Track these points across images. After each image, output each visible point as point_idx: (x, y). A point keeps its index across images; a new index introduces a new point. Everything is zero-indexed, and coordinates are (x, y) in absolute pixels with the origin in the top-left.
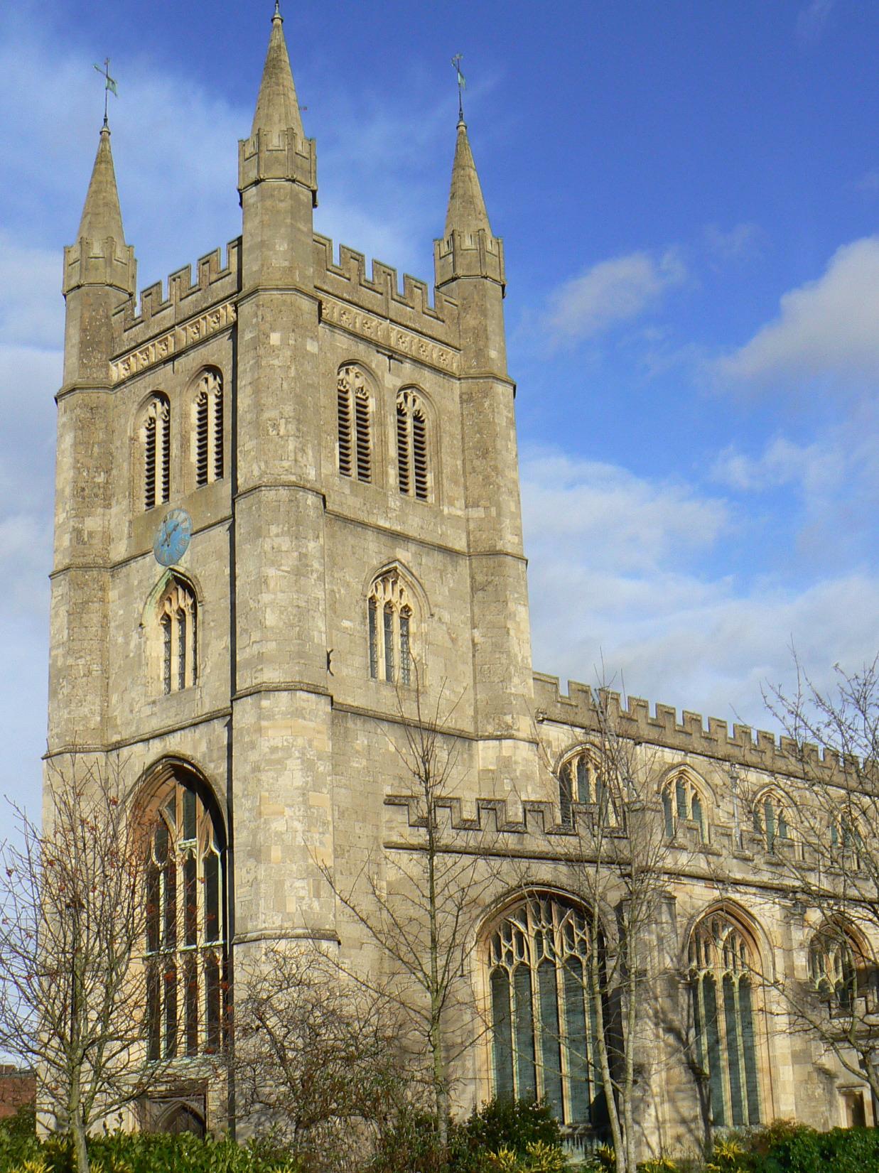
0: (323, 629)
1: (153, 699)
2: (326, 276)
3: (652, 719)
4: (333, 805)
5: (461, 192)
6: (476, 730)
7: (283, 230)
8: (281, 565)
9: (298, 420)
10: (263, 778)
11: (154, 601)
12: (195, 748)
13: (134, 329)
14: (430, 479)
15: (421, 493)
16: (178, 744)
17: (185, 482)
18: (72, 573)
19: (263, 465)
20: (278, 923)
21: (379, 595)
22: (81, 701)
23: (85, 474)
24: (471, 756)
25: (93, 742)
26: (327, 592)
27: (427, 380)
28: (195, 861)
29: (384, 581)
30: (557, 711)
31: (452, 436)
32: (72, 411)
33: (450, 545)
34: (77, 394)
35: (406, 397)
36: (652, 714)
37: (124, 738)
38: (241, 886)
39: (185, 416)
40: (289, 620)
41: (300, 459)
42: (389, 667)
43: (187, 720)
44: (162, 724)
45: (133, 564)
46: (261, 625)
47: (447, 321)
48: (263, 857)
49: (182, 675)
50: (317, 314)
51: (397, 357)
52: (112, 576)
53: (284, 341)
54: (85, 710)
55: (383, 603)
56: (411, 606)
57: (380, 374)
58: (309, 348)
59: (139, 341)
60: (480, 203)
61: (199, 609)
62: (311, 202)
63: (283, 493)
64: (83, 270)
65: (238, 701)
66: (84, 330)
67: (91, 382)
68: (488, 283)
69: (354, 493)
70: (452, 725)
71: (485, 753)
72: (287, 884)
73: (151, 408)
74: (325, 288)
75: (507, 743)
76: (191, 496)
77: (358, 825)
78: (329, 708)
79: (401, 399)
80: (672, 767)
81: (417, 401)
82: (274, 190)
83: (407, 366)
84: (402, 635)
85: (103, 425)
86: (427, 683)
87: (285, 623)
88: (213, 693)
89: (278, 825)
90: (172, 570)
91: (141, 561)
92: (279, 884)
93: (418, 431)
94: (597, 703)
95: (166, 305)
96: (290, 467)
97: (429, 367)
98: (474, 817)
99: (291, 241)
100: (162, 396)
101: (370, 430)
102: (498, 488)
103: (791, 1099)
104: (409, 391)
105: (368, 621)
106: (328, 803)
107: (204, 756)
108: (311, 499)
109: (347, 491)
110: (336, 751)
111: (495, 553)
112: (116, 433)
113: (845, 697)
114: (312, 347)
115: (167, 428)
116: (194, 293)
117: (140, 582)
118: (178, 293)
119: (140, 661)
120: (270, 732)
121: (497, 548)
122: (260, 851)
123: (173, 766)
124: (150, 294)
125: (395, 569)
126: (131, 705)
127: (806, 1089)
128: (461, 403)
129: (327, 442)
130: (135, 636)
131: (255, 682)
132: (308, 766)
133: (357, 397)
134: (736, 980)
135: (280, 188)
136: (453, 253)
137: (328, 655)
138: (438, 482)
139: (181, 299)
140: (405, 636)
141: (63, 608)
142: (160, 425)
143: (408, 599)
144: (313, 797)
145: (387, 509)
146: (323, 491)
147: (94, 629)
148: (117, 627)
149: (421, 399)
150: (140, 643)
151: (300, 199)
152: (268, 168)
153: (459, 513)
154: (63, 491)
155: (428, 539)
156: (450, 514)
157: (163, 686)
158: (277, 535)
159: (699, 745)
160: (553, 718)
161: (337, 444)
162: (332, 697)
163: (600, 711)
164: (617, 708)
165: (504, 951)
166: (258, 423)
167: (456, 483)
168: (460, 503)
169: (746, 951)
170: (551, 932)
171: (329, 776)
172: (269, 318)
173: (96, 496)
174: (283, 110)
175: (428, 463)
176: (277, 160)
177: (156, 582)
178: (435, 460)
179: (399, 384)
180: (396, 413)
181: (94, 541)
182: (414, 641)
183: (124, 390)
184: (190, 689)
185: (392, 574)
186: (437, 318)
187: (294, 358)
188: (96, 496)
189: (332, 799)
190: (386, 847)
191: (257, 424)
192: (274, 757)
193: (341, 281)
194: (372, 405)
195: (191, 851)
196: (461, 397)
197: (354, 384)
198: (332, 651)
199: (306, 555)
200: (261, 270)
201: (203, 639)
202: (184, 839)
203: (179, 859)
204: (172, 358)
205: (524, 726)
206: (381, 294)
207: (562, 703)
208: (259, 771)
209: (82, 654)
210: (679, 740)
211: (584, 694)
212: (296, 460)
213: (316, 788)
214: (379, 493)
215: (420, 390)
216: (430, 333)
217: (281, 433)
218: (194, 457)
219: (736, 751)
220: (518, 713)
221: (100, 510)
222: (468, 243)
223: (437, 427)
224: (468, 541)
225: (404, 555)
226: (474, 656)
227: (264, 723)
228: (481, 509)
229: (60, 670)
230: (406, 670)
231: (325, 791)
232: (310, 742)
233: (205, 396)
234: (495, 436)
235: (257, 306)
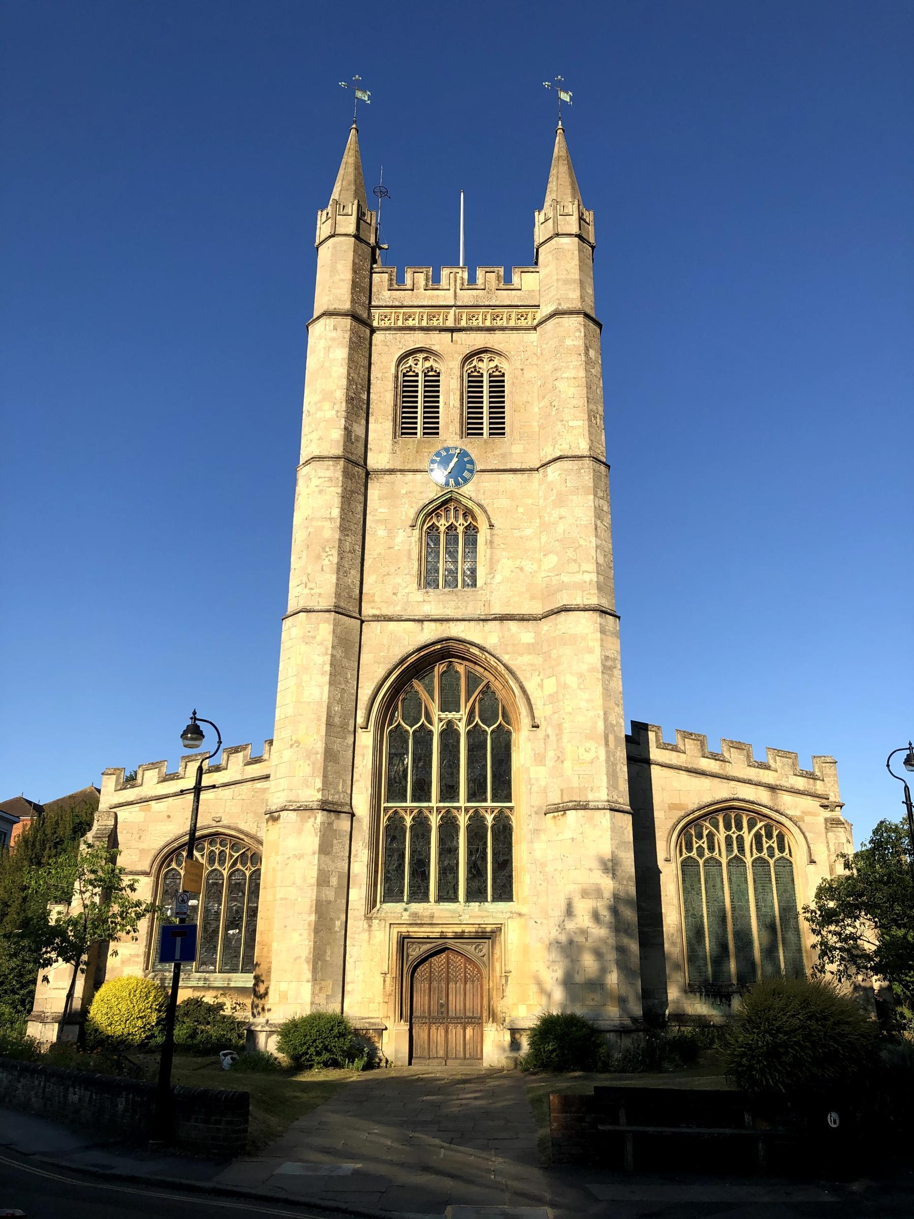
23: (354, 387)
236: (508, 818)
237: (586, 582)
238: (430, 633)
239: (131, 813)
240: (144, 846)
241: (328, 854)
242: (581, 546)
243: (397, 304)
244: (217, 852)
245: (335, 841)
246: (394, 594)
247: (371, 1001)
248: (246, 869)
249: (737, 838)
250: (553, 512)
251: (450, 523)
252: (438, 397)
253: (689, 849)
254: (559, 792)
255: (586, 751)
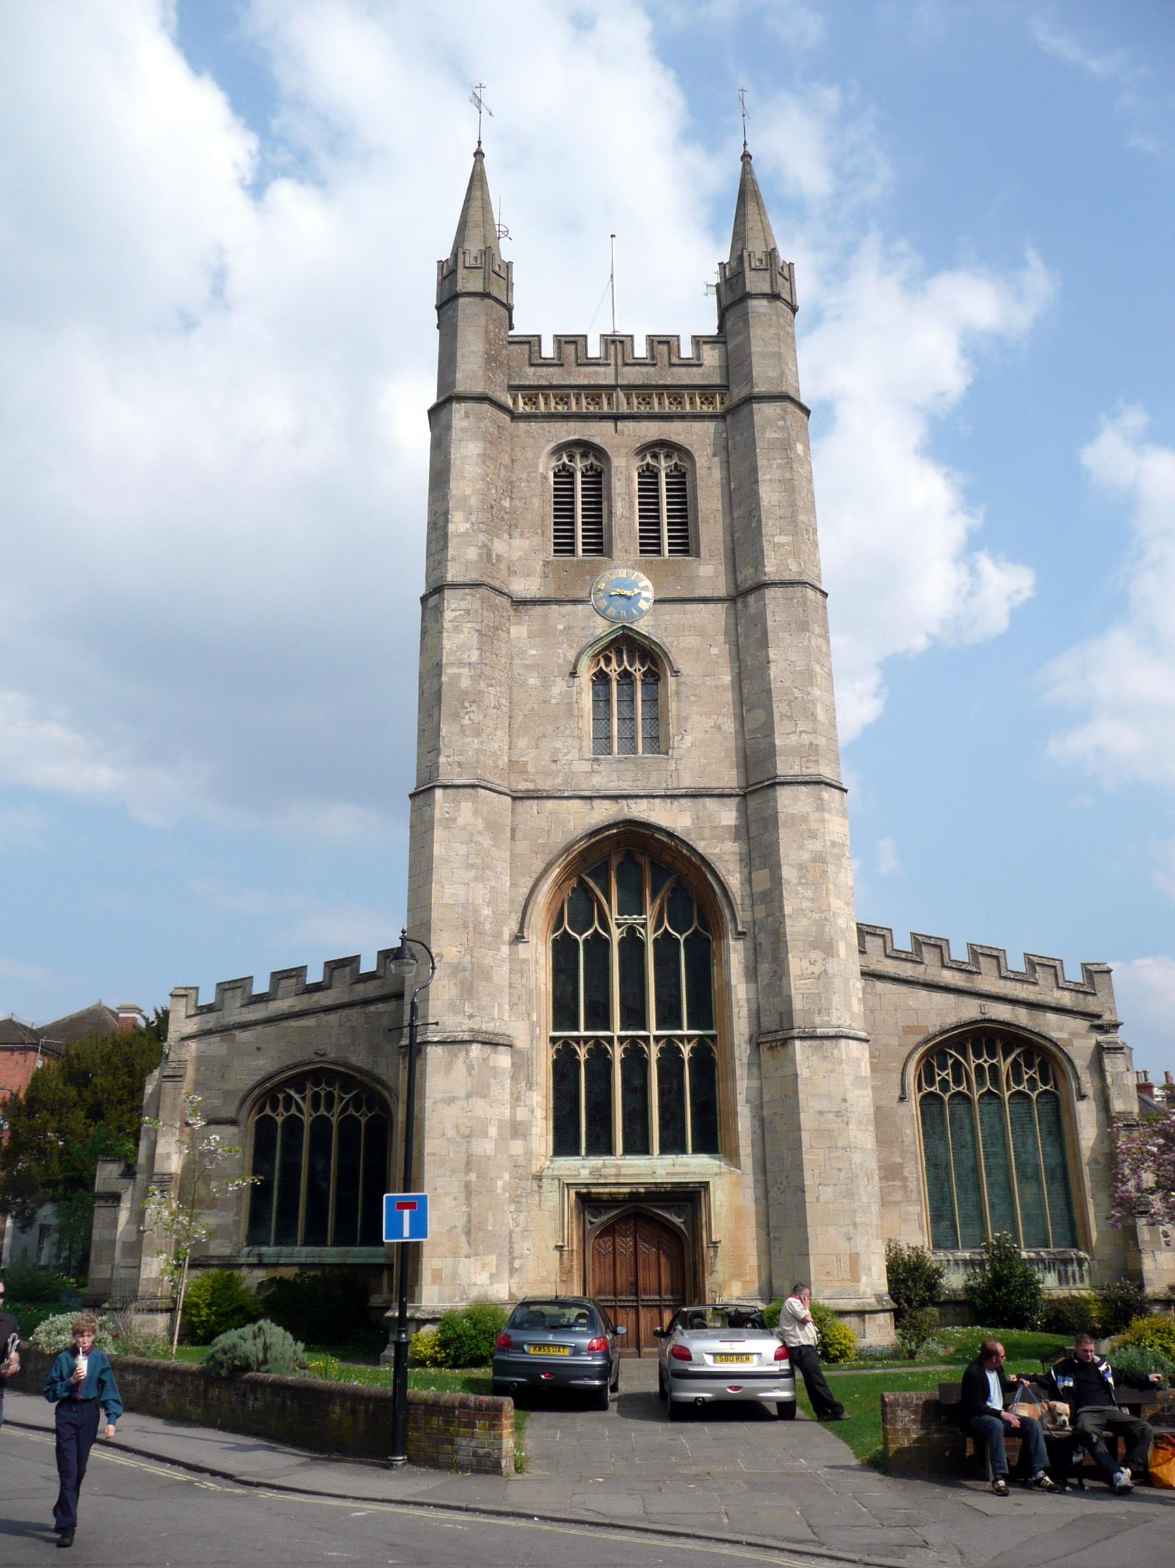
23: (494, 491)
236: (710, 1050)
237: (804, 746)
238: (603, 813)
239: (210, 1044)
240: (229, 1086)
241: (485, 1097)
242: (796, 698)
243: (544, 383)
244: (323, 1093)
245: (492, 1081)
246: (555, 761)
247: (544, 1281)
248: (361, 1115)
249: (989, 1067)
250: (758, 654)
251: (622, 668)
252: (641, 531)
253: (931, 1082)
254: (777, 1017)
255: (811, 964)
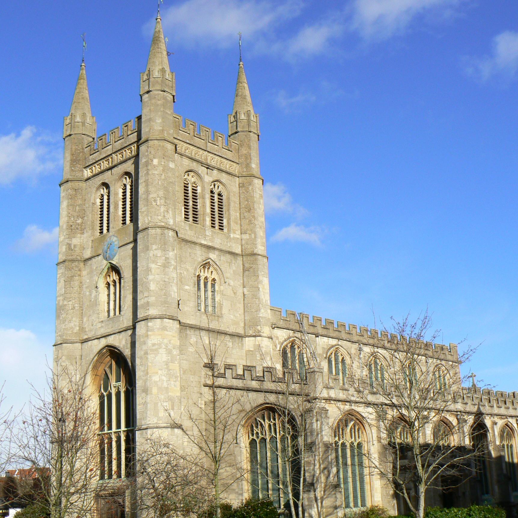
0: (176, 291)
1: (102, 320)
2: (179, 132)
3: (324, 325)
4: (180, 368)
5: (240, 94)
6: (245, 333)
7: (160, 113)
8: (157, 263)
9: (165, 198)
10: (149, 357)
11: (102, 276)
12: (120, 343)
13: (94, 155)
14: (225, 222)
15: (221, 228)
16: (112, 341)
17: (116, 223)
18: (66, 263)
19: (150, 219)
20: (155, 421)
21: (202, 274)
22: (70, 320)
23: (72, 219)
24: (242, 344)
25: (74, 339)
26: (178, 274)
27: (224, 178)
28: (120, 392)
29: (204, 267)
30: (281, 323)
31: (235, 202)
32: (67, 191)
33: (233, 251)
34: (69, 184)
35: (214, 185)
36: (323, 323)
37: (89, 337)
38: (139, 405)
39: (116, 194)
40: (161, 287)
41: (166, 215)
42: (206, 306)
43: (117, 330)
44: (106, 331)
45: (93, 260)
46: (148, 289)
47: (233, 151)
48: (149, 392)
49: (115, 310)
50: (174, 150)
51: (210, 168)
52: (84, 265)
53: (159, 163)
54: (72, 325)
55: (204, 277)
56: (216, 278)
57: (203, 175)
58: (171, 166)
59: (97, 160)
60: (249, 99)
61: (122, 281)
62: (172, 100)
63: (159, 231)
64: (72, 128)
65: (138, 323)
66: (73, 155)
67: (75, 177)
68: (251, 134)
69: (191, 229)
70: (234, 331)
71: (249, 343)
72: (160, 404)
73: (102, 190)
74: (179, 138)
75: (259, 338)
76: (119, 230)
77: (191, 376)
78: (178, 326)
79: (213, 186)
80: (333, 346)
81: (220, 187)
82: (156, 95)
83: (215, 171)
84: (212, 292)
85: (81, 197)
86: (223, 313)
87: (159, 289)
88: (126, 319)
89: (155, 378)
90: (110, 263)
91: (97, 258)
92: (156, 404)
93: (220, 203)
94: (299, 319)
95: (108, 144)
96: (162, 219)
97: (225, 172)
98: (241, 373)
99: (163, 118)
100: (106, 185)
101: (198, 201)
102: (255, 226)
103: (380, 495)
104: (216, 183)
105: (196, 286)
106: (178, 368)
107: (124, 346)
108: (171, 233)
109: (188, 228)
110: (182, 344)
111: (254, 254)
112: (86, 201)
113: (396, 330)
114: (172, 165)
115: (108, 199)
116: (121, 139)
117: (97, 267)
118: (114, 139)
119: (96, 303)
120: (152, 337)
121: (255, 252)
122: (147, 389)
123: (110, 350)
124: (102, 139)
125: (209, 262)
126: (92, 322)
127: (386, 491)
128: (239, 188)
129: (178, 207)
130: (94, 292)
131: (146, 314)
132: (169, 352)
133: (193, 186)
134: (356, 444)
135: (158, 94)
136: (236, 121)
137: (179, 301)
138: (229, 223)
139: (115, 142)
140: (213, 292)
141: (62, 279)
142: (106, 198)
143: (215, 276)
144: (171, 366)
145: (205, 236)
146: (177, 229)
147: (76, 288)
148: (87, 287)
149: (222, 186)
150: (96, 295)
151: (167, 99)
152: (153, 86)
153: (238, 236)
154: (63, 226)
155: (224, 248)
156: (234, 237)
157: (106, 314)
158: (156, 250)
159: (344, 335)
160: (279, 326)
161: (183, 208)
162: (180, 321)
163: (300, 323)
164: (308, 321)
165: (255, 432)
166: (148, 199)
167: (237, 223)
168: (239, 232)
169: (360, 432)
170: (275, 424)
171: (178, 355)
172: (153, 153)
173: (77, 229)
174: (160, 60)
175: (224, 214)
176: (157, 82)
177: (103, 268)
178: (227, 213)
179: (211, 180)
180: (210, 193)
181: (76, 249)
182: (217, 294)
183: (90, 182)
184: (118, 316)
185: (207, 264)
186: (229, 150)
187: (163, 170)
188: (77, 229)
189: (180, 366)
190: (204, 386)
191: (147, 200)
192: (154, 348)
193: (185, 135)
194: (199, 190)
195: (119, 388)
196: (239, 185)
197: (191, 180)
198: (180, 300)
199: (168, 258)
200: (149, 131)
201: (124, 294)
202: (116, 382)
203: (113, 392)
204: (111, 168)
205: (266, 330)
206: (204, 140)
207: (283, 320)
208: (147, 354)
209: (70, 299)
210: (336, 334)
211: (293, 316)
212: (164, 216)
213: (172, 362)
214: (202, 229)
215: (221, 182)
216: (225, 157)
217: (158, 204)
218: (120, 213)
219: (361, 338)
220: (263, 325)
221: (79, 235)
222: (243, 117)
223: (228, 199)
224: (242, 249)
225: (213, 256)
226: (244, 300)
227: (149, 333)
228: (248, 235)
229: (61, 307)
230: (214, 307)
231: (176, 362)
232: (170, 341)
233: (125, 185)
234: (254, 203)
235: (148, 147)
253: (253, 435)
